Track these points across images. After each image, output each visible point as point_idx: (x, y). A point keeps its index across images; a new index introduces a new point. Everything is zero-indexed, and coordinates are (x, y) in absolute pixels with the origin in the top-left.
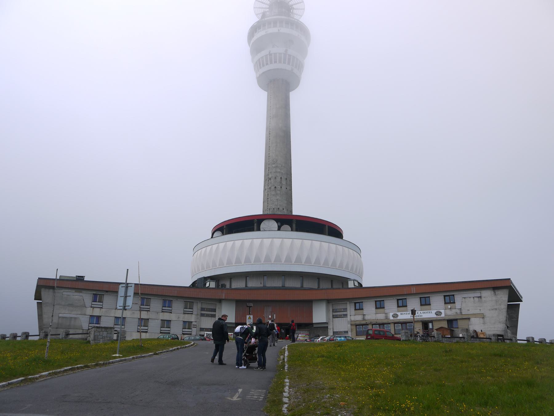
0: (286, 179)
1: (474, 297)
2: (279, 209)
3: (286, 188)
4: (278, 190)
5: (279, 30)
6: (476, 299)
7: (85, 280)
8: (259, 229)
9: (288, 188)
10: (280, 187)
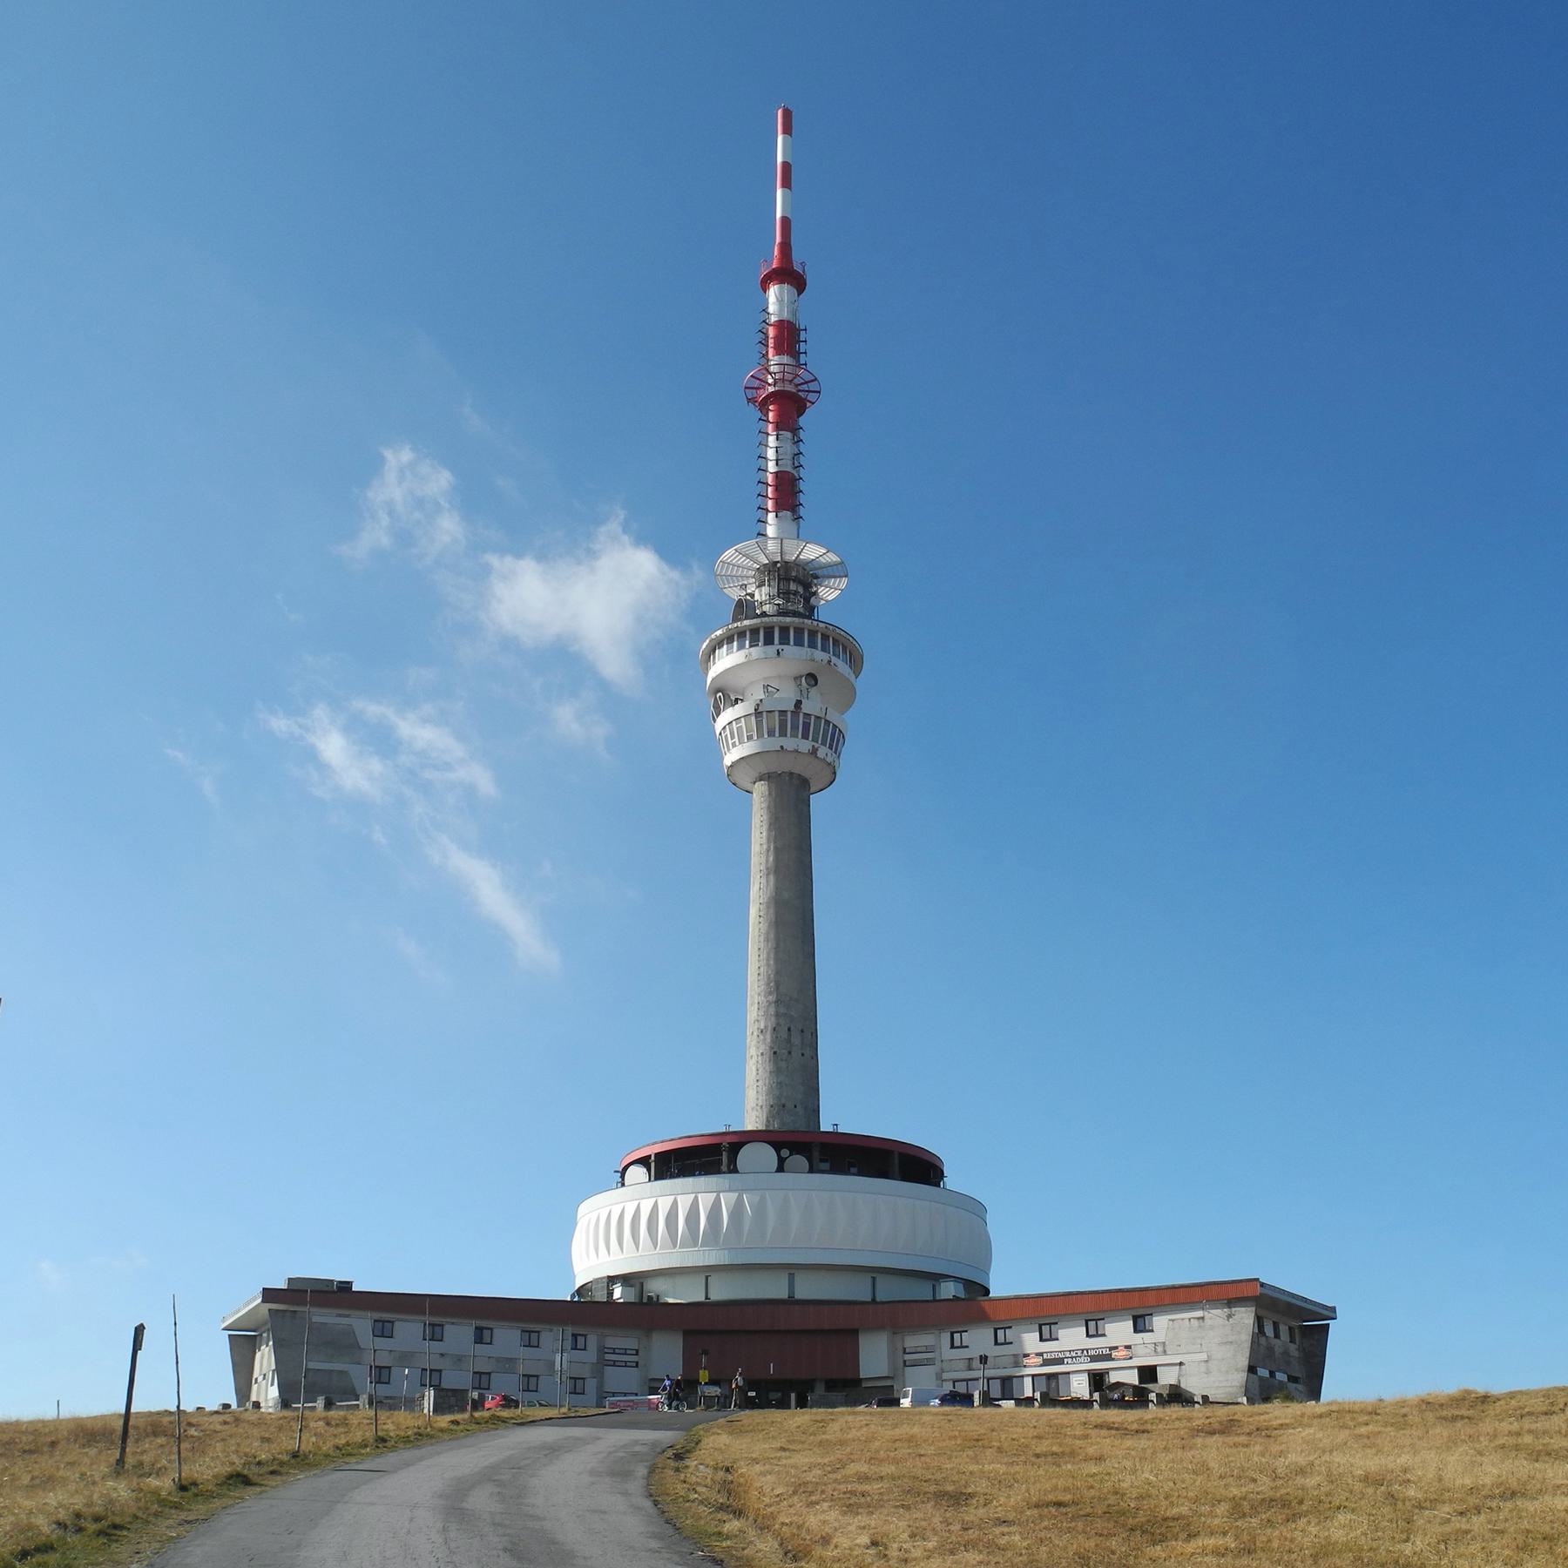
0: (802, 1031)
2: (784, 1106)
3: (803, 1055)
4: (782, 1060)
8: (733, 1169)
9: (808, 1053)
10: (785, 1052)
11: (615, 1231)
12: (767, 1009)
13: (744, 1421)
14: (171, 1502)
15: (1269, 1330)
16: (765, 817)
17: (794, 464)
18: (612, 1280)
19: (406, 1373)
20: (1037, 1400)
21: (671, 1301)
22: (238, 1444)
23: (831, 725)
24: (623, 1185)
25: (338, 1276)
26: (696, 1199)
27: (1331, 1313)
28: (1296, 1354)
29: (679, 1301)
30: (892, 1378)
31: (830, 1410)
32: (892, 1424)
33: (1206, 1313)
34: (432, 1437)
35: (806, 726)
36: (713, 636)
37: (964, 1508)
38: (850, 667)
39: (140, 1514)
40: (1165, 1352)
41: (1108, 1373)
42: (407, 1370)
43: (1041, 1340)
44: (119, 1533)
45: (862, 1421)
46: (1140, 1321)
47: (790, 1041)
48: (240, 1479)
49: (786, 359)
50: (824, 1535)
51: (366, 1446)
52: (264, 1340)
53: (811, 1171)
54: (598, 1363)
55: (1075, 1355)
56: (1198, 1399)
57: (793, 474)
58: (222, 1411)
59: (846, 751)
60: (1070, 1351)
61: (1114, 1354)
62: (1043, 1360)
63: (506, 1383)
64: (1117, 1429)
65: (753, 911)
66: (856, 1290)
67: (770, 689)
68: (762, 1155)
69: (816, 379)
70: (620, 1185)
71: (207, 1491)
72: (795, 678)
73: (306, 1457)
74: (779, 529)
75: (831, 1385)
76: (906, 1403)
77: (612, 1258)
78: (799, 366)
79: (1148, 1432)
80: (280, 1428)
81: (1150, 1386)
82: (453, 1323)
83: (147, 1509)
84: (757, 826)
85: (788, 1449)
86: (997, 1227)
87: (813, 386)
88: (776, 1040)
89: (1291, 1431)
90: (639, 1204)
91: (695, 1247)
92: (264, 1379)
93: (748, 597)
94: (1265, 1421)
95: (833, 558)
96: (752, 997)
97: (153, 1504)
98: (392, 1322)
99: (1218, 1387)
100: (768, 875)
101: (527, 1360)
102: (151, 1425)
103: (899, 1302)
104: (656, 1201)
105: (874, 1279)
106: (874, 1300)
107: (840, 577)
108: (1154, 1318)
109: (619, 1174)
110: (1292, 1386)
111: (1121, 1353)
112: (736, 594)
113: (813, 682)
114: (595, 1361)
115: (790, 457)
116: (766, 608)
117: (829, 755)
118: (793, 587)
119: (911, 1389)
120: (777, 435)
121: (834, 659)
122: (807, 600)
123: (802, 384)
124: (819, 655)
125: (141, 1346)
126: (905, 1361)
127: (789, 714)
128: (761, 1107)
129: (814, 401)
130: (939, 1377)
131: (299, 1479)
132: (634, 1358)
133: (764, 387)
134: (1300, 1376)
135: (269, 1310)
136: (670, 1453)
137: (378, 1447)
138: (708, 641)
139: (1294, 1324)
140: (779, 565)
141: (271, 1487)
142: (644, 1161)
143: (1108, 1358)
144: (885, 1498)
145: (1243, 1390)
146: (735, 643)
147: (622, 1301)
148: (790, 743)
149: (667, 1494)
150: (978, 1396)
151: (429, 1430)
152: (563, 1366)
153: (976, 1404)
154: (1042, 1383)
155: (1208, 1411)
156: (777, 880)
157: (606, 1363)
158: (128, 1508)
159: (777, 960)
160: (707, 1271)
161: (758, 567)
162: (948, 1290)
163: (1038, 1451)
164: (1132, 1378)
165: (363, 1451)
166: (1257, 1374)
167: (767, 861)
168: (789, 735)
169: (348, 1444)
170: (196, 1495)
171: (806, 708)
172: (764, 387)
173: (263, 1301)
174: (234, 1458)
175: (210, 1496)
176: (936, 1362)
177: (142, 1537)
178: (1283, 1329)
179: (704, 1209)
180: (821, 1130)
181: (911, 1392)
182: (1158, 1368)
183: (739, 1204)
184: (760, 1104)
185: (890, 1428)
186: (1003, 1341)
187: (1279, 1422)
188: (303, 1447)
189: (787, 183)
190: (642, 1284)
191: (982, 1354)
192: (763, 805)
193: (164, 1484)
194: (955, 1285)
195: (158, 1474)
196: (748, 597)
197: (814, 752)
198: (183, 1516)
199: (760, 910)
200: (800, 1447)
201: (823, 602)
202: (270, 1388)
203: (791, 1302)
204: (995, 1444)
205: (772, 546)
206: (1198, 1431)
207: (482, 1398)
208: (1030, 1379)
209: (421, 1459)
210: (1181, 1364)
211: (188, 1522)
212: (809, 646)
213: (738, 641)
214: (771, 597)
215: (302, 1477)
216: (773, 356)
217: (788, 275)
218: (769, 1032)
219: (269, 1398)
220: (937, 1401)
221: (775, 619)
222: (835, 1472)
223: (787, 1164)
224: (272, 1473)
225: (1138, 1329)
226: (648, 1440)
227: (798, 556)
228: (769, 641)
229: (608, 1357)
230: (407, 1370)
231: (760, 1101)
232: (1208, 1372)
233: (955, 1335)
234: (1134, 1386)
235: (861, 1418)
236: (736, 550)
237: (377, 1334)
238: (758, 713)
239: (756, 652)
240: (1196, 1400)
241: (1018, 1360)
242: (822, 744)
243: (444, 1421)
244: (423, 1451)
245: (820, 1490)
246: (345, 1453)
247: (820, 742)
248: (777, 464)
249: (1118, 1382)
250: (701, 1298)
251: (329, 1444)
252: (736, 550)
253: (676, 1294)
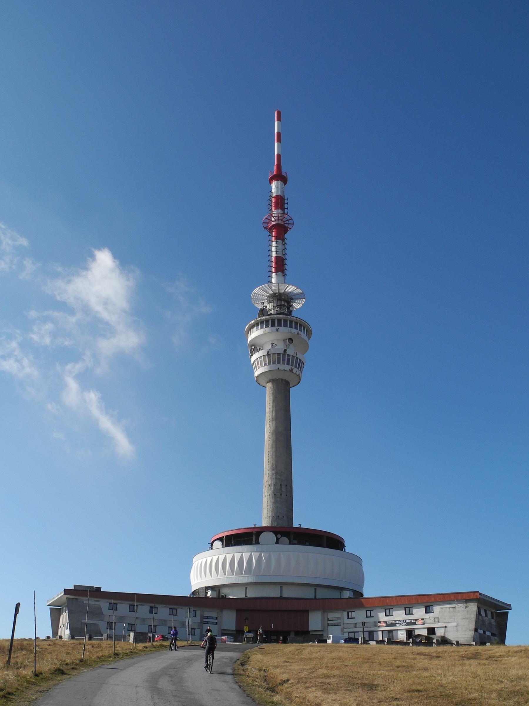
0: (286, 485)
1: (449, 608)
2: (278, 517)
3: (286, 495)
4: (278, 497)
6: (452, 609)
7: (102, 591)
8: (258, 543)
10: (279, 494)
11: (208, 568)
12: (272, 476)
13: (266, 649)
14: (32, 682)
15: (483, 613)
16: (271, 397)
17: (283, 253)
18: (207, 588)
19: (124, 625)
20: (386, 641)
21: (231, 597)
22: (57, 655)
23: (299, 359)
24: (212, 549)
25: (96, 585)
26: (242, 555)
27: (509, 607)
28: (494, 624)
29: (234, 597)
30: (323, 631)
31: (301, 644)
32: (330, 651)
33: (456, 605)
34: (137, 653)
35: (288, 360)
36: (250, 323)
37: (375, 691)
38: (306, 335)
39: (19, 688)
40: (439, 622)
41: (414, 630)
42: (125, 624)
43: (386, 615)
44: (10, 696)
45: (317, 650)
46: (428, 608)
47: (281, 490)
48: (60, 671)
49: (279, 211)
50: (317, 703)
51: (110, 657)
52: (64, 611)
53: (290, 543)
54: (200, 622)
55: (400, 622)
56: (454, 642)
57: (283, 257)
58: (47, 639)
59: (305, 370)
60: (398, 621)
61: (417, 622)
62: (386, 624)
63: (162, 630)
64: (427, 655)
65: (266, 436)
66: (308, 594)
67: (274, 345)
68: (270, 537)
69: (292, 219)
70: (210, 549)
71: (47, 677)
72: (284, 340)
73: (86, 661)
74: (277, 280)
75: (297, 633)
76: (329, 641)
77: (207, 579)
78: (285, 213)
79: (441, 657)
80: (73, 648)
81: (432, 636)
82: (141, 605)
83: (22, 685)
84: (268, 401)
85: (288, 662)
86: (366, 568)
87: (290, 222)
88: (275, 489)
89: (506, 658)
90: (219, 557)
91: (242, 575)
92: (64, 626)
93: (264, 308)
94: (492, 653)
95: (299, 291)
96: (266, 471)
97: (24, 682)
99: (461, 637)
100: (272, 421)
101: (173, 621)
102: (20, 645)
103: (326, 599)
104: (226, 556)
105: (315, 589)
106: (315, 598)
107: (302, 299)
108: (434, 607)
109: (210, 545)
110: (493, 638)
111: (420, 622)
112: (259, 306)
113: (291, 342)
114: (200, 622)
115: (281, 250)
116: (272, 312)
117: (298, 372)
118: (283, 303)
119: (332, 636)
120: (276, 242)
121: (300, 332)
122: (289, 308)
123: (286, 221)
124: (294, 331)
125: (18, 612)
126: (328, 624)
127: (281, 355)
128: (269, 517)
129: (291, 228)
130: (342, 630)
131: (84, 672)
132: (216, 621)
133: (270, 223)
134: (496, 633)
135: (67, 598)
136: (239, 663)
137: (116, 658)
138: (248, 325)
139: (493, 611)
140: (277, 294)
141: (73, 675)
142: (221, 539)
143: (414, 624)
144: (339, 686)
145: (473, 639)
146: (259, 326)
147: (211, 597)
148: (282, 367)
149: (244, 682)
150: (361, 639)
151: (135, 650)
152: (189, 624)
153: (360, 642)
154: (386, 634)
155: (459, 648)
156: (276, 423)
157: (204, 622)
158: (14, 685)
159: (276, 456)
160: (246, 585)
161: (269, 295)
162: (347, 594)
163: (396, 665)
164: (425, 633)
165: (109, 659)
166: (478, 632)
167: (272, 415)
168: (281, 363)
169: (103, 656)
170: (42, 679)
171: (289, 352)
172: (270, 223)
173: (64, 594)
174: (56, 661)
175: (47, 679)
176: (341, 625)
177: (20, 699)
178: (489, 613)
179: (246, 560)
180: (294, 526)
181: (332, 637)
183: (260, 557)
184: (269, 515)
185: (329, 653)
186: (370, 616)
187: (499, 654)
188: (84, 657)
189: (279, 141)
190: (219, 590)
191: (363, 621)
192: (271, 392)
193: (28, 673)
194: (349, 592)
195: (24, 668)
196: (264, 308)
197: (291, 370)
198: (37, 688)
199: (269, 436)
200: (293, 661)
201: (295, 309)
202: (66, 630)
203: (281, 598)
204: (377, 661)
205: (274, 287)
206: (463, 657)
207: (154, 636)
208: (381, 632)
209: (135, 663)
210: (446, 627)
211: (40, 692)
212: (290, 327)
213: (260, 325)
214: (274, 307)
215: (85, 671)
216: (274, 210)
217: (280, 177)
218: (272, 486)
219: (65, 634)
220: (343, 641)
221: (276, 316)
222: (313, 673)
223: (279, 541)
224: (73, 668)
225: (427, 612)
226: (228, 656)
227: (285, 290)
228: (273, 325)
230: (125, 624)
231: (268, 514)
232: (457, 631)
233: (349, 613)
234: (426, 636)
235: (316, 648)
236: (260, 288)
237: (131, 611)
238: (268, 355)
239: (268, 330)
240: (453, 643)
241: (376, 624)
242: (295, 367)
243: (140, 646)
244: (135, 660)
245: (309, 681)
246: (102, 660)
247: (294, 366)
248: (276, 253)
249: (419, 634)
250: (244, 596)
251: (95, 656)
252: (260, 288)
253: (233, 595)
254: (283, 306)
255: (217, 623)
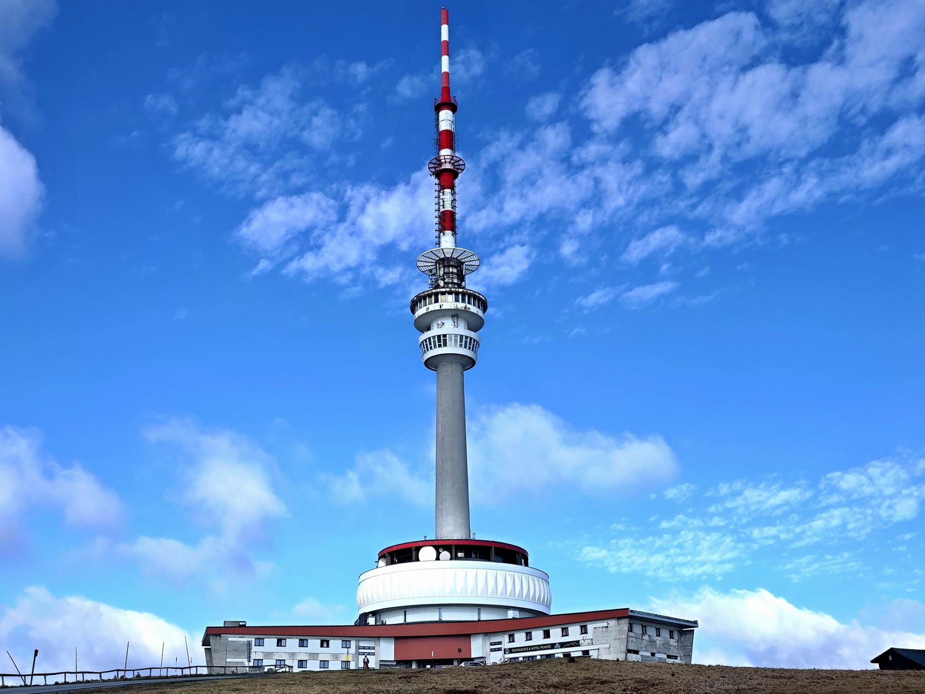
5: (441, 307)
66: (470, 616)
82: (290, 638)
98: (263, 639)
121: (468, 306)
182: (590, 651)
210: (598, 649)
229: (360, 651)
254: (451, 274)
255: (374, 654)
